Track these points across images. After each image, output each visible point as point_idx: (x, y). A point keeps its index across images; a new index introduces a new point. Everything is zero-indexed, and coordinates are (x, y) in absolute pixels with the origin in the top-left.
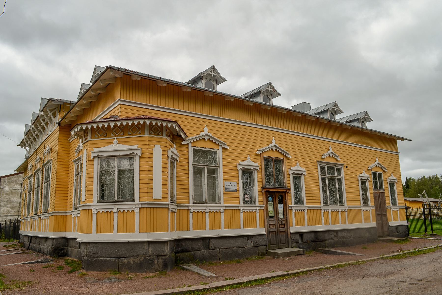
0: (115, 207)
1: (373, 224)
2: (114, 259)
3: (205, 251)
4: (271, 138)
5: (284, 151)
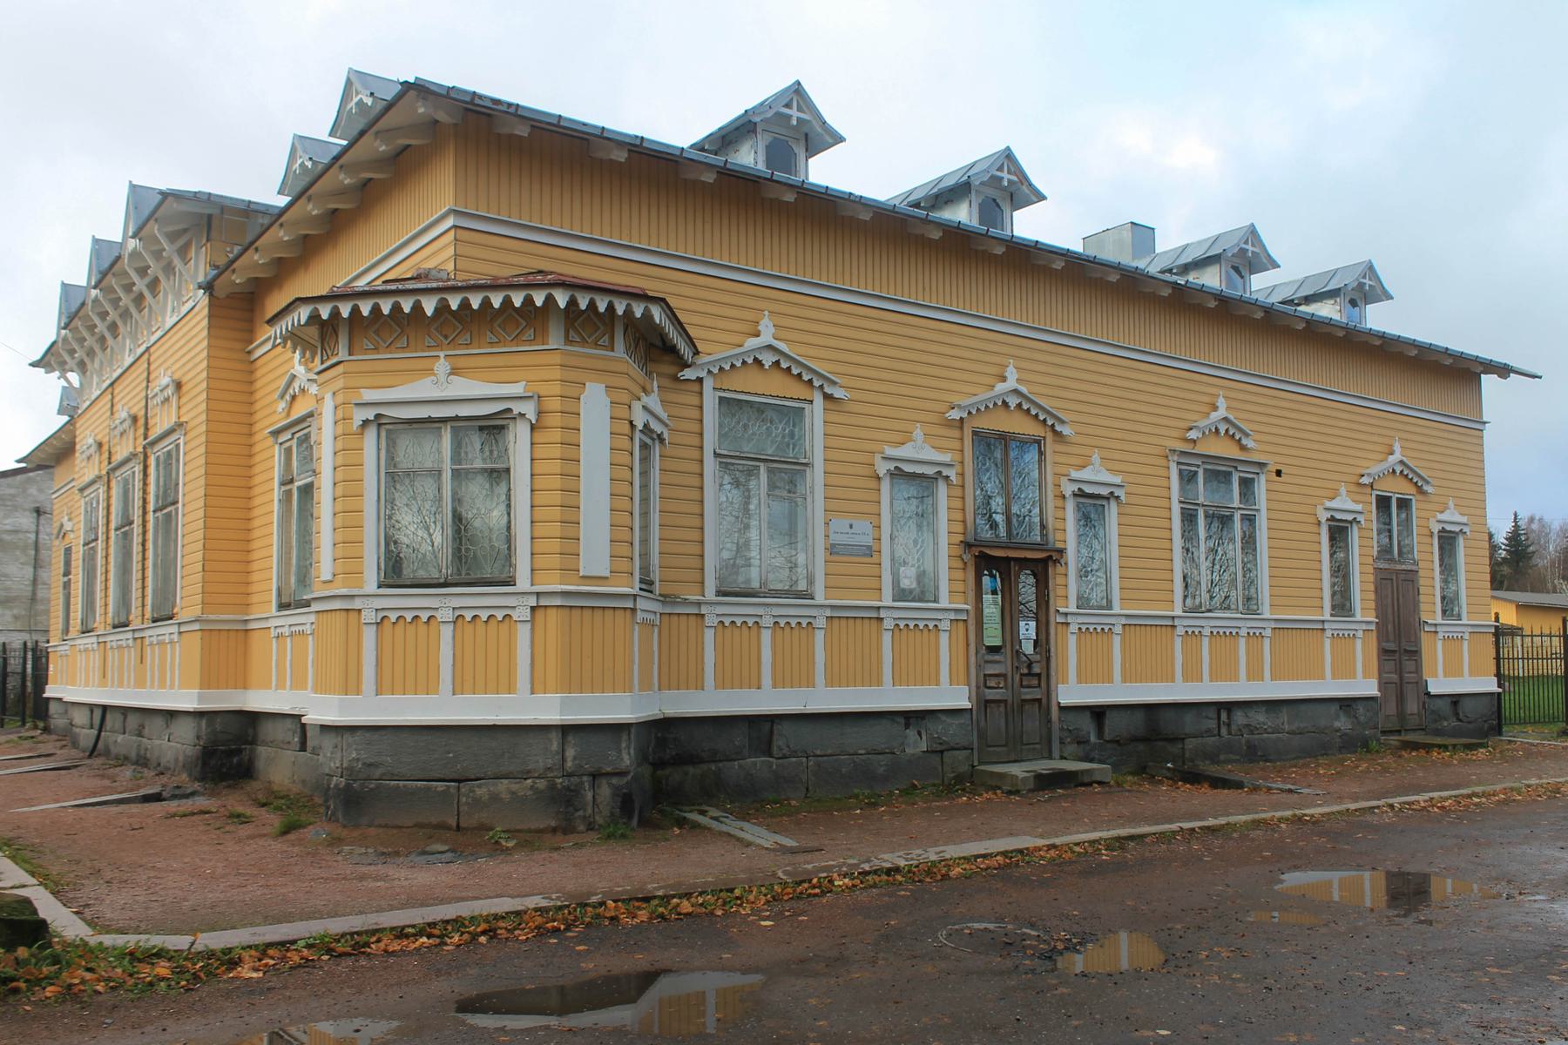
0: (443, 605)
1: (1368, 687)
2: (440, 786)
3: (757, 763)
4: (1003, 357)
5: (1048, 412)
